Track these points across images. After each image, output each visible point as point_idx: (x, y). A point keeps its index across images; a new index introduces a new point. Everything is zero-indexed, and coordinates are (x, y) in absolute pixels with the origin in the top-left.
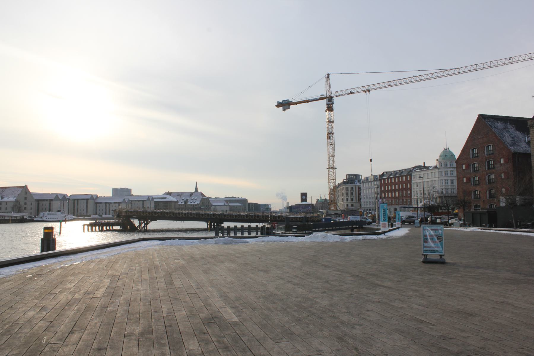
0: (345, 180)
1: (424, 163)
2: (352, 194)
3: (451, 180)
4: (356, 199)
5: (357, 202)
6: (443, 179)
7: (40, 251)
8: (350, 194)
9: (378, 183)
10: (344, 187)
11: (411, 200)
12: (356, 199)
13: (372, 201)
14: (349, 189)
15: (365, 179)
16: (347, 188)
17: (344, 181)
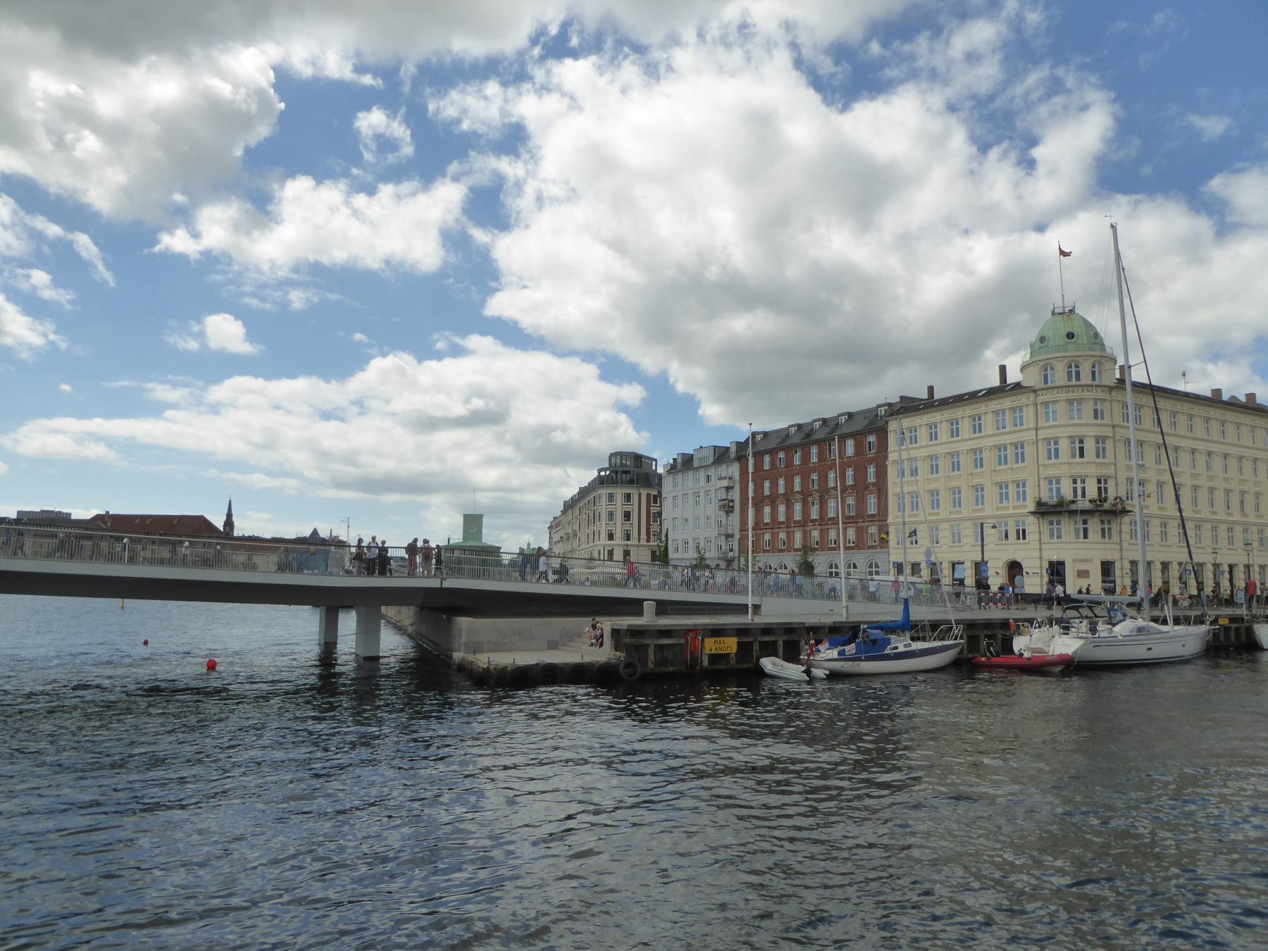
0: (605, 470)
1: (931, 389)
2: (627, 516)
3: (1072, 439)
4: (639, 535)
5: (643, 542)
6: (1063, 433)
7: (485, 520)
8: (619, 516)
9: (735, 470)
10: (603, 492)
11: (884, 530)
12: (639, 535)
13: (1165, 566)
14: (619, 499)
15: (679, 461)
16: (611, 497)
17: (603, 473)
